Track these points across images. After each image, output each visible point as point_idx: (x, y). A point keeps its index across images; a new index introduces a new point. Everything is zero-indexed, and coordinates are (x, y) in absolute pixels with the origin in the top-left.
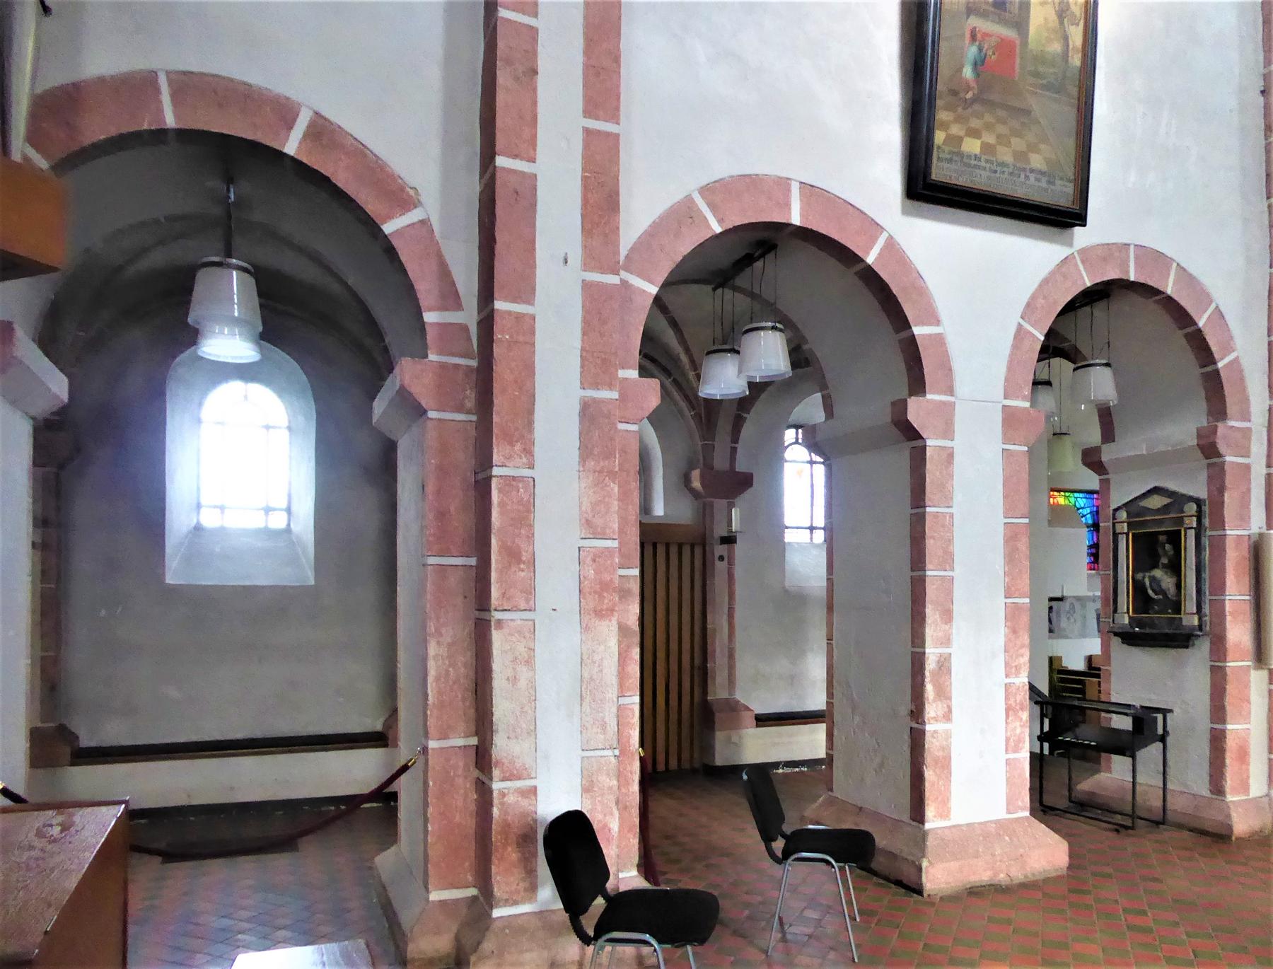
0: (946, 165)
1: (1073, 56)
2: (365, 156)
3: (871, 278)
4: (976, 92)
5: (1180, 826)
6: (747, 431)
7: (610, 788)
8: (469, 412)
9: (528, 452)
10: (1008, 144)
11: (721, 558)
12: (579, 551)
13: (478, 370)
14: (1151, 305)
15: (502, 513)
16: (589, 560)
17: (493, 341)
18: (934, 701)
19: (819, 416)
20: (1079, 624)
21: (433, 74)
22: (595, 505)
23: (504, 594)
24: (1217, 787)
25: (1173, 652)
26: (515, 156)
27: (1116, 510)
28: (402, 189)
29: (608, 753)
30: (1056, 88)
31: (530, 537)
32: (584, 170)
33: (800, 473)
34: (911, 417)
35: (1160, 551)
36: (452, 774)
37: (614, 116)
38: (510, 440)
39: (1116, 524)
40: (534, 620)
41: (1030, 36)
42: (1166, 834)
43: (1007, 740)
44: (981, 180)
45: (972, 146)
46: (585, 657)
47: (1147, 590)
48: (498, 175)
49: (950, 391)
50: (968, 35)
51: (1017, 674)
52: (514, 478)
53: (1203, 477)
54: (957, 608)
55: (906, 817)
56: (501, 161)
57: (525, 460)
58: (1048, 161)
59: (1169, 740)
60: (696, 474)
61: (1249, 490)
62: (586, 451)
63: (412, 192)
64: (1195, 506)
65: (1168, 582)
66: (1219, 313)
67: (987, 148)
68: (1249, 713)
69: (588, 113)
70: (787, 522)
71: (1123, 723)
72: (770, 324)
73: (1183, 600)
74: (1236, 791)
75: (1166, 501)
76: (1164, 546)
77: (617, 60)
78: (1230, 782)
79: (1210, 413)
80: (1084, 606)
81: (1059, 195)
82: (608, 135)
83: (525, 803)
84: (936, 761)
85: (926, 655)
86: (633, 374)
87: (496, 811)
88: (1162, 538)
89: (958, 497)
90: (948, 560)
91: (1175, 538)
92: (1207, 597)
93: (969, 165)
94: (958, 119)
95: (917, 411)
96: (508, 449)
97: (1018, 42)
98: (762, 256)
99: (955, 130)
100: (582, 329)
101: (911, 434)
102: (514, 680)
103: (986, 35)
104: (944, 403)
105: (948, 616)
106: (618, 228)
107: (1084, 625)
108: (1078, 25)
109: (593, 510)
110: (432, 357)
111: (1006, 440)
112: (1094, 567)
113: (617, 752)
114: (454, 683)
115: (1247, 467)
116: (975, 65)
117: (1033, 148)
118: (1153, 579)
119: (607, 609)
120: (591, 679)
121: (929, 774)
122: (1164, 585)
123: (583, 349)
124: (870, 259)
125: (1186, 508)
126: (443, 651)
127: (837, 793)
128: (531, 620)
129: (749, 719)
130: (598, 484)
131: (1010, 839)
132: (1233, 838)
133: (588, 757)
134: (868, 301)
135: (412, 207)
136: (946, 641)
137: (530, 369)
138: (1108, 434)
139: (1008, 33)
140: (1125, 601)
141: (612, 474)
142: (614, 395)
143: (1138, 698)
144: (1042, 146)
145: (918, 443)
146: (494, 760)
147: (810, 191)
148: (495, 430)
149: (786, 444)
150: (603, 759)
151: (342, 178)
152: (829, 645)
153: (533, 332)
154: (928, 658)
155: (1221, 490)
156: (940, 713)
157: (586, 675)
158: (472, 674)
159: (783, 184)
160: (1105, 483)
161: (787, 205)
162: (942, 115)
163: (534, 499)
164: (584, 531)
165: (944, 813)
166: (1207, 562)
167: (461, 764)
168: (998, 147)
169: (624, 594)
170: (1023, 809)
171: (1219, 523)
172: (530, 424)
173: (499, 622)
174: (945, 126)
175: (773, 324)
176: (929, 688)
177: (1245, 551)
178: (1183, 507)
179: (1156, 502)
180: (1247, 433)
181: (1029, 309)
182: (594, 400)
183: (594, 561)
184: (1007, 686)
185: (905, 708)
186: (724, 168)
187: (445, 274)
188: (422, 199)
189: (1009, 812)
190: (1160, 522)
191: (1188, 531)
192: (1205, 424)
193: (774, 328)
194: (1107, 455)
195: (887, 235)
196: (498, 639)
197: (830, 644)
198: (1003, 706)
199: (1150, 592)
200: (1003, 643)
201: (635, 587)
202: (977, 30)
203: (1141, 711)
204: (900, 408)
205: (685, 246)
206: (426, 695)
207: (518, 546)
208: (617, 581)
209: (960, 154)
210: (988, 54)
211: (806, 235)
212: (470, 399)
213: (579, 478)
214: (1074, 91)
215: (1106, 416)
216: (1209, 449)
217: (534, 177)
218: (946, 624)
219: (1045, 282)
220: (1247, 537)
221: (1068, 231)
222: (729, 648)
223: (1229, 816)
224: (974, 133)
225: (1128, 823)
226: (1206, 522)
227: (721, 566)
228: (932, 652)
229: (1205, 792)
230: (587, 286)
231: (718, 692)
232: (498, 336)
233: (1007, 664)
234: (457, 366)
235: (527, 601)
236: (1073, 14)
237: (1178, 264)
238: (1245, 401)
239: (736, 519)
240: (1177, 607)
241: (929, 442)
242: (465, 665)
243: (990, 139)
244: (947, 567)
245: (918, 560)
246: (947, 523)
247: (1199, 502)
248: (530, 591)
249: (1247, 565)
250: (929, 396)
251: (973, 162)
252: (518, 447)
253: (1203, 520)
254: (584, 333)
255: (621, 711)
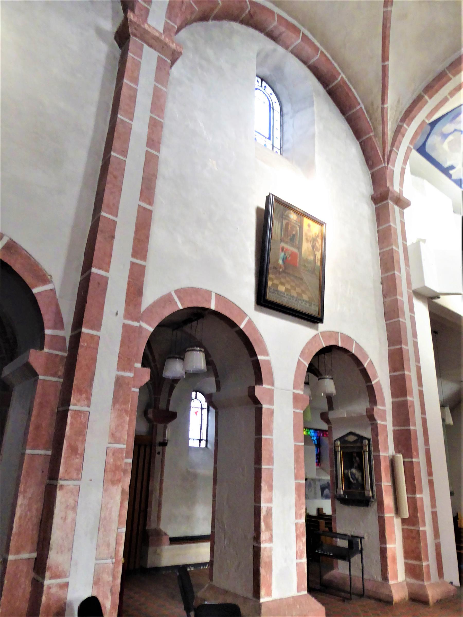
0: (272, 294)
1: (317, 262)
2: (30, 259)
3: (241, 334)
4: (283, 269)
5: (369, 597)
6: (175, 392)
7: (108, 582)
8: (59, 377)
9: (89, 399)
10: (295, 289)
11: (159, 453)
12: (107, 449)
13: (68, 357)
14: (346, 356)
15: (71, 428)
16: (111, 454)
17: (79, 346)
18: (265, 530)
19: (213, 389)
20: (313, 491)
21: (67, 231)
22: (117, 427)
23: (66, 471)
24: (385, 577)
25: (362, 508)
26: (100, 269)
27: (335, 441)
28: (45, 275)
29: (109, 561)
30: (313, 272)
31: (84, 441)
32: (129, 277)
33: (196, 413)
34: (256, 394)
35: (354, 460)
36: (19, 576)
37: (144, 258)
38: (80, 392)
40: (80, 486)
41: (302, 252)
42: (365, 601)
43: (297, 552)
44: (284, 301)
45: (282, 288)
46: (103, 506)
47: (350, 478)
48: (91, 275)
49: (272, 384)
50: (280, 249)
51: (301, 518)
52: (80, 411)
53: (369, 429)
54: (275, 483)
55: (250, 595)
56: (94, 270)
57: (86, 402)
58: (309, 298)
59: (363, 552)
60: (150, 411)
61: (387, 436)
62: (116, 400)
63: (49, 277)
64: (367, 441)
66: (371, 362)
67: (287, 290)
68: (395, 539)
69: (133, 256)
70: (190, 438)
71: (343, 544)
72: (198, 349)
73: (365, 483)
74: (393, 579)
76: (356, 459)
77: (148, 237)
78: (390, 574)
79: (371, 402)
80: (315, 483)
81: (313, 311)
82: (141, 265)
83: (60, 592)
84: (266, 563)
85: (262, 508)
86: (139, 365)
87: (44, 598)
88: (355, 455)
89: (275, 431)
90: (271, 461)
91: (360, 455)
92: (375, 483)
93: (280, 295)
94: (277, 278)
95: (259, 391)
96: (79, 397)
97: (298, 254)
98: (197, 319)
99: (276, 282)
100: (120, 344)
101: (256, 402)
102: (65, 519)
103: (287, 250)
104: (269, 389)
105: (271, 488)
106: (141, 303)
107: (315, 493)
108: (319, 251)
109: (116, 429)
110: (46, 350)
111: (295, 407)
112: (319, 464)
113: (114, 560)
114: (29, 520)
115: (386, 426)
116: (283, 260)
117: (303, 292)
118: (352, 473)
119: (117, 480)
120: (105, 518)
121: (263, 571)
123: (119, 353)
124: (242, 327)
125: (364, 442)
126: (26, 502)
127: (214, 583)
128: (78, 485)
129: (167, 541)
130: (120, 416)
131: (300, 607)
132: (394, 603)
133: (98, 564)
134: (240, 343)
135: (48, 282)
136: (270, 500)
137: (94, 360)
138: (331, 407)
139: (295, 250)
140: (341, 483)
141: (126, 412)
142: (132, 375)
143: (349, 531)
144: (307, 292)
145: (259, 406)
146: (47, 567)
147: (218, 297)
148: (74, 387)
149: (192, 399)
150: (106, 565)
151: (17, 267)
152: (214, 501)
153: (98, 343)
154: (262, 509)
155: (377, 435)
156: (268, 538)
157: (103, 516)
158: (40, 516)
159: (209, 293)
160: (330, 428)
161: (210, 301)
162: (270, 276)
163: (88, 422)
164: (110, 439)
165: (269, 593)
166: (373, 467)
167: (25, 570)
168: (291, 291)
169: (125, 471)
170: (304, 590)
171: (377, 449)
172: (91, 384)
173: (62, 486)
174: (272, 280)
175: (200, 349)
176: (263, 524)
177: (388, 463)
178: (362, 442)
179: (351, 438)
180: (385, 411)
181: (302, 354)
182: (122, 376)
183: (113, 454)
184: (296, 524)
185: (251, 534)
186: (185, 284)
187: (58, 313)
188: (53, 280)
190: (352, 447)
192: (369, 406)
193: (200, 351)
194: (332, 415)
195: (248, 318)
196: (60, 495)
197: (214, 500)
198: (294, 534)
199: (352, 480)
200: (294, 502)
201: (130, 469)
202: (284, 247)
203: (351, 538)
204: (251, 391)
205: (167, 312)
206: (11, 528)
207: (77, 446)
208: (123, 465)
209: (277, 290)
210: (288, 257)
211: (216, 314)
212: (61, 370)
213: (111, 412)
214: (318, 274)
215: (330, 399)
216: (371, 417)
217: (107, 278)
218: (270, 492)
219: (308, 343)
220: (388, 457)
221: (316, 325)
222: (159, 501)
223: (391, 591)
224: (283, 284)
225: (348, 596)
226: (372, 449)
227: (158, 457)
228: (264, 505)
229: (380, 579)
230: (124, 326)
231: (152, 525)
232: (81, 343)
233: (296, 513)
234: (57, 355)
235: (78, 474)
236: (317, 248)
237: (356, 342)
238: (383, 398)
239: (368, 473)
240: (363, 486)
241: (264, 406)
242: (37, 510)
243: (289, 287)
244: (271, 463)
245: (258, 460)
246: (271, 443)
247: (369, 440)
248: (79, 469)
249: (389, 469)
250: (264, 386)
251: (282, 295)
252: (84, 396)
253: (371, 448)
254: (121, 346)
255: (118, 535)
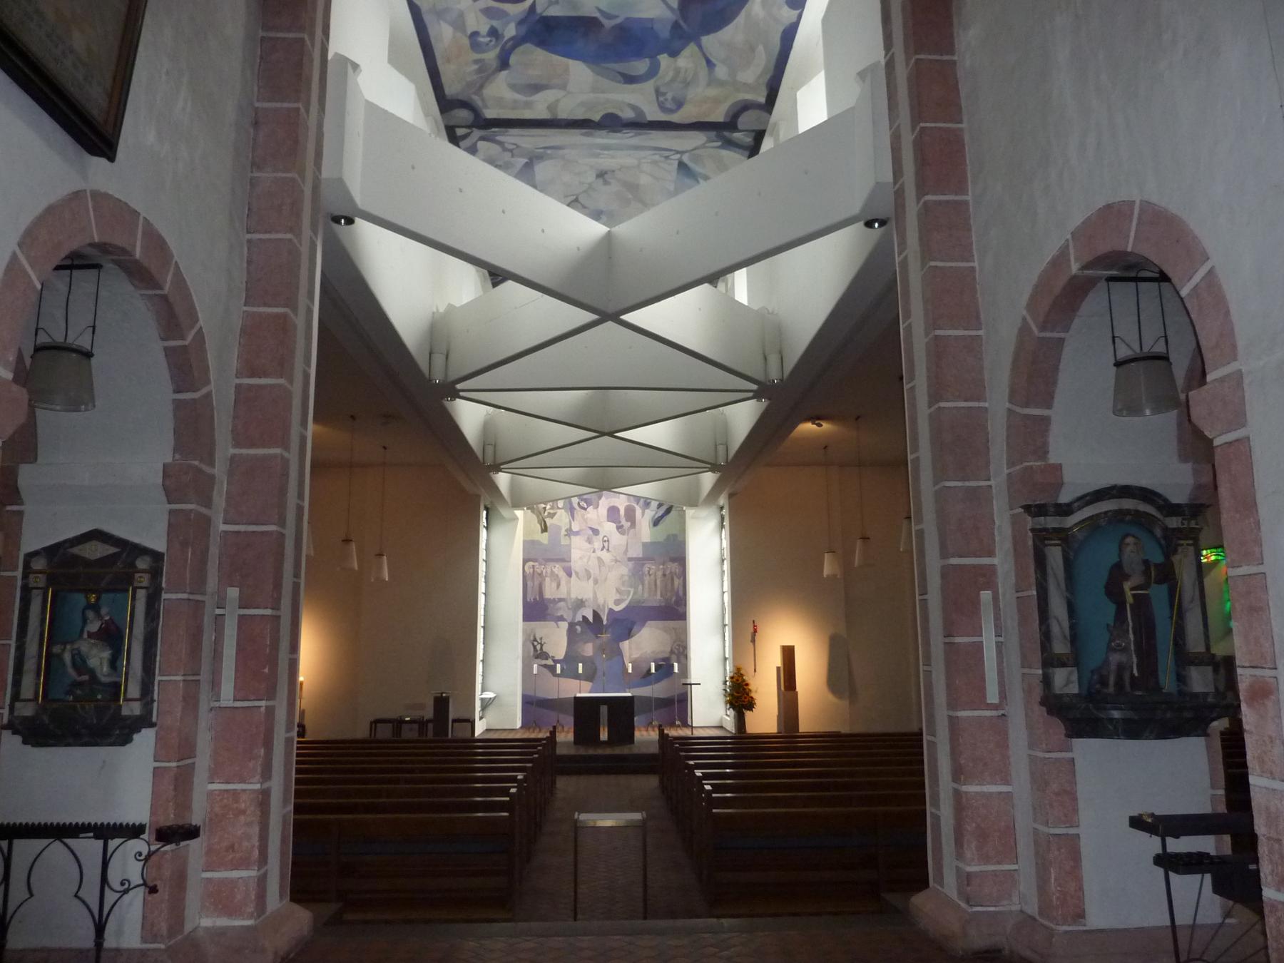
27: (30, 556)
39: (138, 590)
65: (98, 658)
75: (112, 550)
122: (93, 662)
189: (144, 940)
191: (138, 590)
195: (568, 543)
247: (157, 557)
